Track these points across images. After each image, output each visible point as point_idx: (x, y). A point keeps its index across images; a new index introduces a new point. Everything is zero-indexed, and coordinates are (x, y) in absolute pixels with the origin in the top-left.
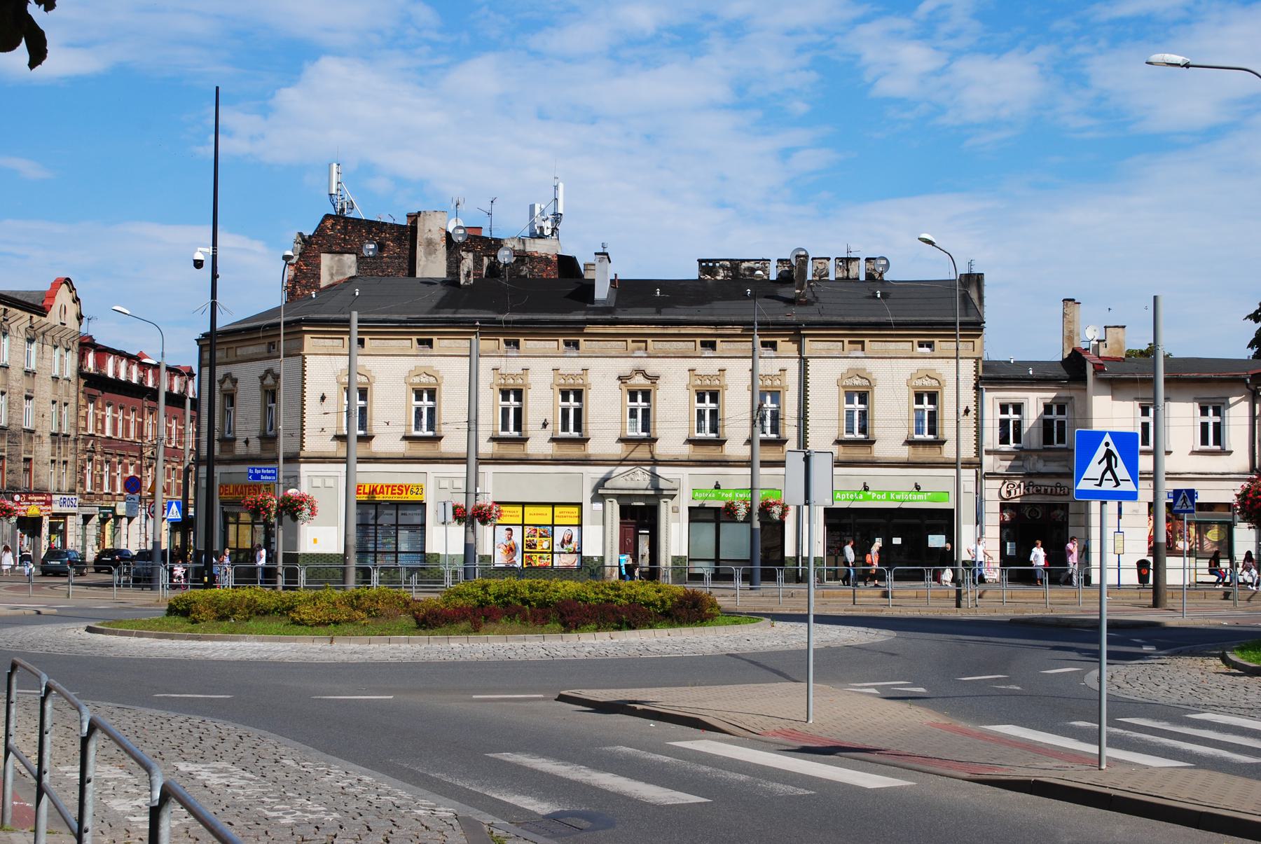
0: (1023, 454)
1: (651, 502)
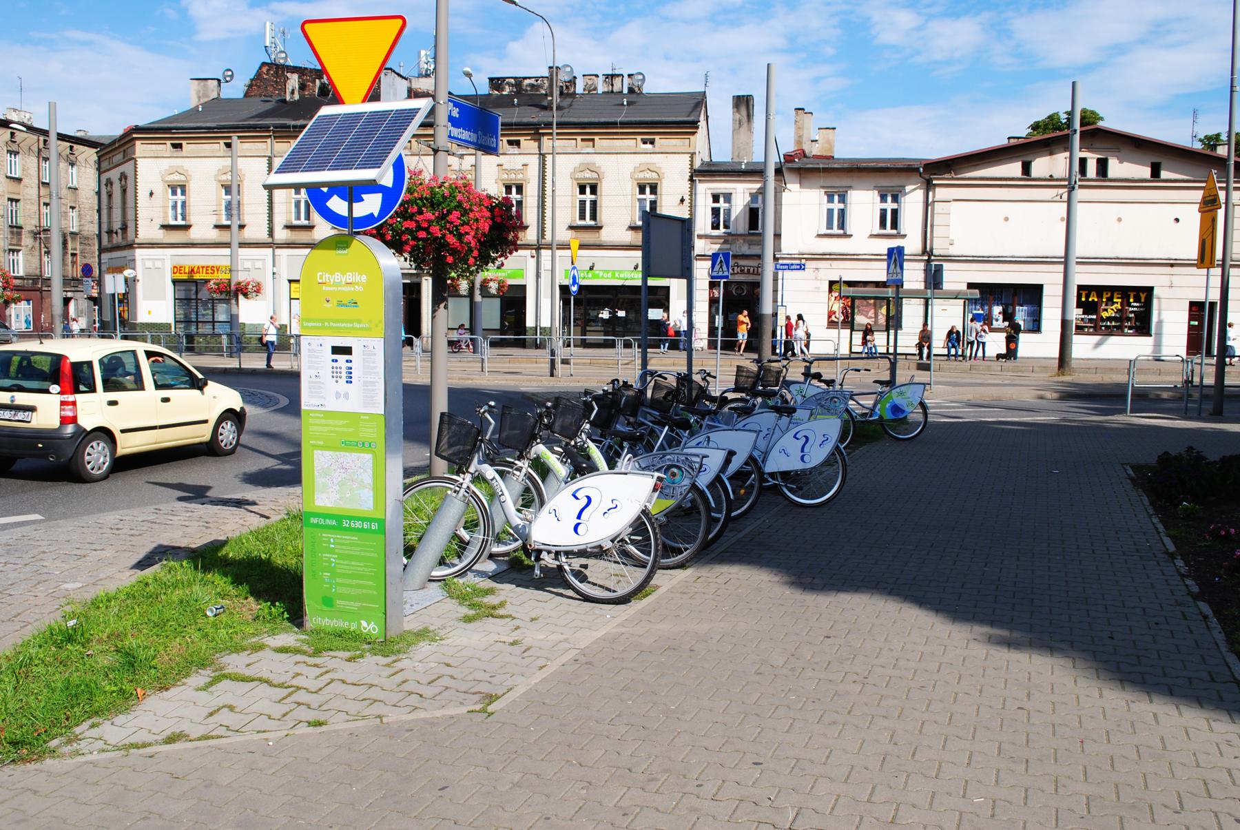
1: (415, 280)
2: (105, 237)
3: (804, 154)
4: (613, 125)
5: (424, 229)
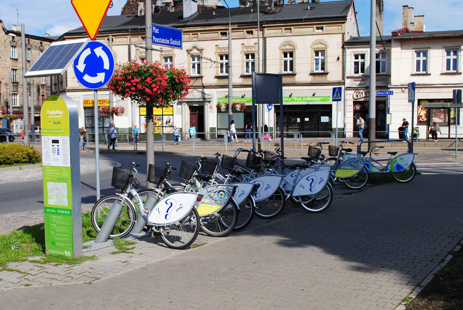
0: (364, 78)
1: (201, 104)
2: (53, 86)
3: (407, 30)
4: (301, 20)
5: (134, 86)
